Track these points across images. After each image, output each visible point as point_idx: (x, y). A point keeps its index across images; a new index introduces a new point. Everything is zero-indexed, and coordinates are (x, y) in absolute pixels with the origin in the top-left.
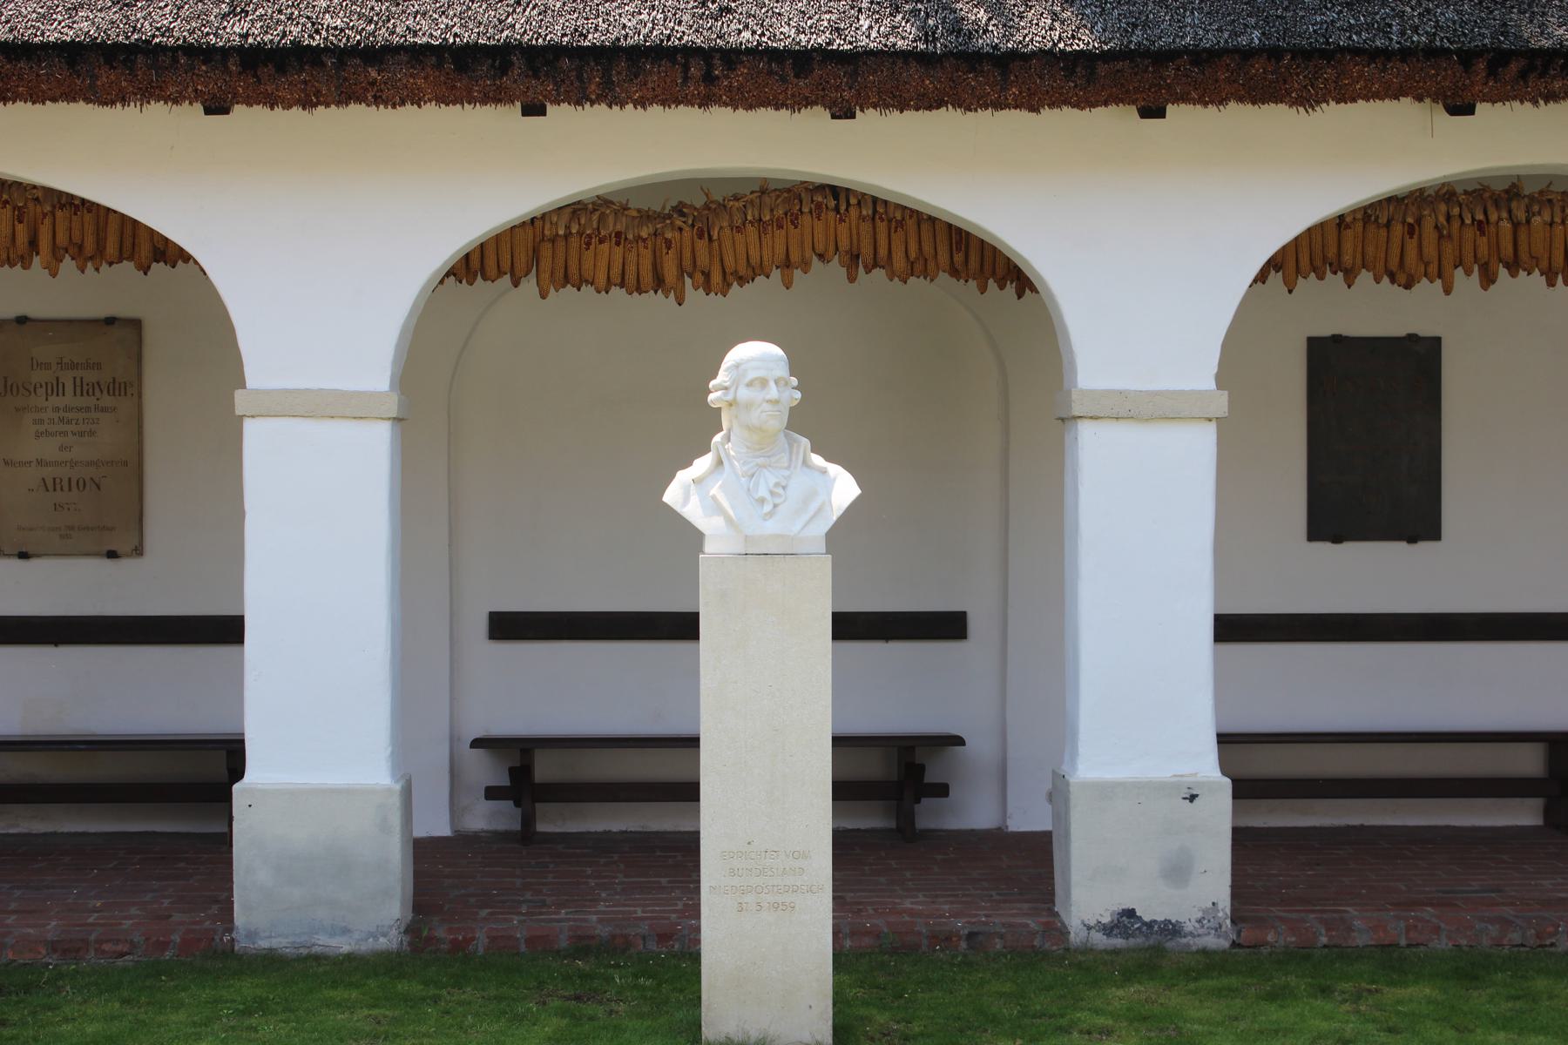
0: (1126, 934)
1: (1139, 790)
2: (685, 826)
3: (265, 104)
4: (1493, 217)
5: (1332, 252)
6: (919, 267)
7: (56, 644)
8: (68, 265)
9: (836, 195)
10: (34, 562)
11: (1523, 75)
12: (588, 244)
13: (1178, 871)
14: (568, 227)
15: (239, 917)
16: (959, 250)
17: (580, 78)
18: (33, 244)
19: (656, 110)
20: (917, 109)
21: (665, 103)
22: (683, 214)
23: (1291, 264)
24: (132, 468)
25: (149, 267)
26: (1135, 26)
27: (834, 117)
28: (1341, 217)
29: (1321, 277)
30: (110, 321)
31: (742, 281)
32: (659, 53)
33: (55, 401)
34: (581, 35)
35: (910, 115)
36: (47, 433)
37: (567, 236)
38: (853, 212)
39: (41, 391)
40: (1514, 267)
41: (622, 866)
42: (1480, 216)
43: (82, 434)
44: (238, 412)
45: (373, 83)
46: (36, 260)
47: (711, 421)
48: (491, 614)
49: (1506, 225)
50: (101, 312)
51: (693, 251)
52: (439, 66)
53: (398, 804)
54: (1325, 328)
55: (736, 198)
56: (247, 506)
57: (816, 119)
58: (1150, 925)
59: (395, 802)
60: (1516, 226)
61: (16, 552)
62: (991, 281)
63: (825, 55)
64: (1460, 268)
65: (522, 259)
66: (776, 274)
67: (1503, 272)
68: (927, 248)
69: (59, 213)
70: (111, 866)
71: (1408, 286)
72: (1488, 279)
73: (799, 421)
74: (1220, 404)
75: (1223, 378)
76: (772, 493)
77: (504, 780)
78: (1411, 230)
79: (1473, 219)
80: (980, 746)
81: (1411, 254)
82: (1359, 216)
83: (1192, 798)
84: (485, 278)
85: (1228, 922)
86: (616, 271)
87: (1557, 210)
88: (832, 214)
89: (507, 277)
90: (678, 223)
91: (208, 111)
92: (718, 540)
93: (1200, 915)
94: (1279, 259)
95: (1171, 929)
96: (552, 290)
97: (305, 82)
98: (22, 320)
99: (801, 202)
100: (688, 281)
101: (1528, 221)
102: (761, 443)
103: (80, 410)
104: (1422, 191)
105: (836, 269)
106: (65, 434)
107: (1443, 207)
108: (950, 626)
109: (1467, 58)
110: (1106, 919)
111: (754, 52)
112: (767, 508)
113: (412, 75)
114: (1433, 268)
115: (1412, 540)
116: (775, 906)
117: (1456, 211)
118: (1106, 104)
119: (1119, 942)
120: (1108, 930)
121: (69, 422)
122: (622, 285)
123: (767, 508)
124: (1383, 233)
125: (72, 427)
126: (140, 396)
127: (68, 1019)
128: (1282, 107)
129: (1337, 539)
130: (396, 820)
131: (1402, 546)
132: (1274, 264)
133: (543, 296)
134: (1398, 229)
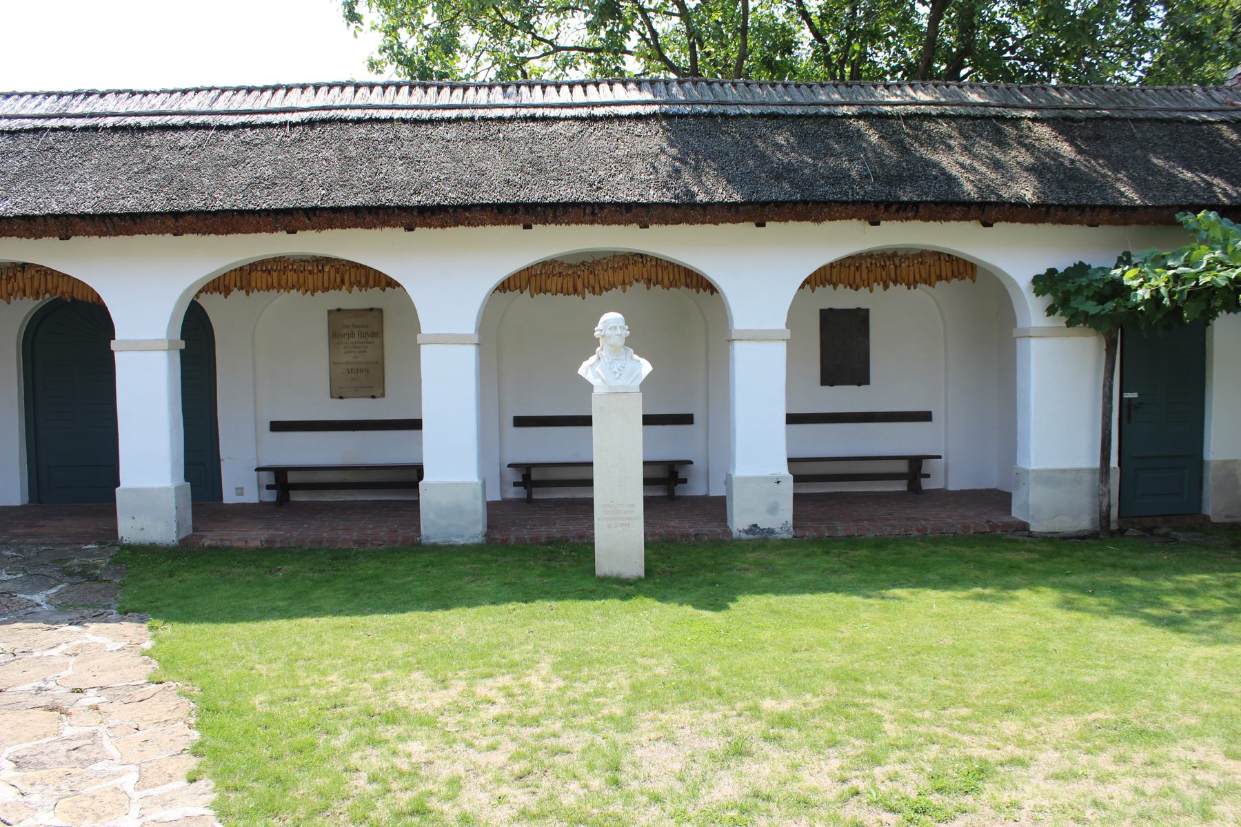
4: (888, 264)
6: (673, 284)
7: (354, 430)
8: (355, 289)
10: (345, 400)
11: (897, 211)
12: (269, 273)
13: (773, 510)
17: (545, 214)
18: (343, 282)
19: (573, 226)
23: (814, 282)
24: (380, 365)
29: (824, 286)
30: (371, 310)
31: (607, 290)
32: (575, 205)
35: (669, 226)
37: (541, 274)
40: (895, 282)
42: (883, 264)
44: (419, 342)
45: (467, 218)
46: (344, 287)
47: (596, 343)
48: (515, 417)
49: (892, 266)
50: (367, 306)
55: (604, 259)
57: (634, 228)
58: (763, 530)
59: (480, 488)
60: (896, 267)
63: (637, 205)
67: (891, 284)
68: (677, 277)
71: (857, 290)
73: (629, 342)
74: (788, 335)
77: (521, 480)
78: (857, 268)
80: (699, 464)
83: (778, 482)
84: (510, 290)
90: (583, 268)
95: (771, 531)
98: (339, 310)
100: (586, 290)
101: (900, 265)
103: (361, 343)
104: (861, 254)
105: (642, 285)
107: (869, 260)
108: (687, 419)
109: (877, 204)
110: (746, 528)
112: (618, 375)
114: (866, 283)
116: (622, 525)
117: (874, 262)
119: (751, 537)
120: (747, 532)
122: (562, 292)
123: (618, 375)
124: (847, 269)
126: (382, 337)
128: (809, 223)
129: (832, 385)
130: (480, 494)
131: (855, 387)
133: (532, 297)
134: (853, 268)
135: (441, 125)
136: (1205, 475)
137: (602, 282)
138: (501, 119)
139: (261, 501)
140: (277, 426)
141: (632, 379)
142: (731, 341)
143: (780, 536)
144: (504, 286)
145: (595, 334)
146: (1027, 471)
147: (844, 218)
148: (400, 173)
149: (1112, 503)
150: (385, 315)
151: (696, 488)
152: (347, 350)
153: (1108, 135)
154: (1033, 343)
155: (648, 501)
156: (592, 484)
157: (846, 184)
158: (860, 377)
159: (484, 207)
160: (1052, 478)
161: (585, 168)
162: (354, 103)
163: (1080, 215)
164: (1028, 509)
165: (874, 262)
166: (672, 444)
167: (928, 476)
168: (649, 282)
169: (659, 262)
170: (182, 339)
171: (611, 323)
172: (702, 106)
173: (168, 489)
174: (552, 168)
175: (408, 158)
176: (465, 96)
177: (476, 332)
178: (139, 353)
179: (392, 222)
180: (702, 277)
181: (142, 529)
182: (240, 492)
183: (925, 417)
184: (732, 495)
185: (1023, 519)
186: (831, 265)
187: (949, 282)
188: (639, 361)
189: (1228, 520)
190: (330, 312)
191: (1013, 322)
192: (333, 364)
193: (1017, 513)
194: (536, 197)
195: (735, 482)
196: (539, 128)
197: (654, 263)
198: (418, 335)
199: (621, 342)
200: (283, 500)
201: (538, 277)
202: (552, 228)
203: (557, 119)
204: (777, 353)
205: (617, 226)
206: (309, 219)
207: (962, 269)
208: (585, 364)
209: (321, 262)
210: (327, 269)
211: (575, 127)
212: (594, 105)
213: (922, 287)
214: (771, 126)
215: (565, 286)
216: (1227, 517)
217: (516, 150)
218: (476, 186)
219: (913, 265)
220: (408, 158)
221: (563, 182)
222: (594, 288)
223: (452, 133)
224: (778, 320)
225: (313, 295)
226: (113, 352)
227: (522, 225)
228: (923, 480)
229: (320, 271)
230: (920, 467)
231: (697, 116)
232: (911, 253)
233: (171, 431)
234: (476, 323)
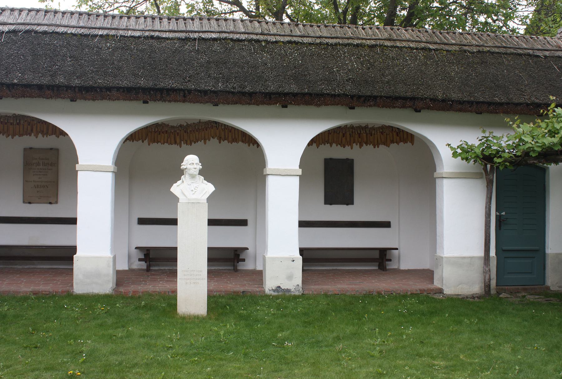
0: (278, 292)
1: (281, 260)
3: (84, 99)
4: (362, 132)
6: (234, 140)
8: (40, 135)
11: (364, 101)
12: (159, 134)
13: (290, 277)
14: (155, 129)
16: (244, 137)
18: (32, 130)
20: (232, 104)
22: (181, 127)
25: (59, 136)
26: (280, 87)
27: (213, 106)
29: (325, 145)
30: (51, 149)
32: (174, 90)
34: (156, 85)
40: (367, 144)
41: (166, 276)
42: (359, 132)
43: (44, 175)
44: (77, 169)
45: (108, 95)
46: (33, 134)
48: (138, 218)
49: (365, 135)
50: (50, 147)
51: (183, 135)
53: (112, 260)
54: (328, 157)
56: (78, 191)
58: (283, 290)
59: (111, 260)
61: (28, 202)
62: (251, 144)
64: (355, 144)
67: (364, 145)
69: (38, 124)
70: (69, 285)
73: (201, 173)
74: (300, 172)
76: (195, 189)
77: (143, 257)
78: (344, 135)
79: (358, 133)
80: (251, 251)
82: (333, 131)
83: (293, 261)
85: (301, 289)
87: (375, 131)
88: (215, 128)
89: (141, 141)
91: (71, 101)
92: (182, 199)
93: (295, 287)
95: (288, 290)
96: (151, 143)
97: (93, 95)
98: (31, 148)
99: (208, 124)
103: (44, 169)
104: (346, 126)
106: (40, 175)
107: (351, 130)
108: (243, 223)
109: (352, 97)
111: (196, 90)
112: (193, 192)
113: (117, 94)
115: (347, 204)
117: (354, 131)
119: (276, 294)
120: (274, 291)
121: (41, 172)
123: (193, 192)
126: (58, 166)
129: (331, 204)
130: (111, 264)
132: (311, 143)
133: (149, 145)
134: (341, 134)
136: (547, 262)
143: (293, 293)
145: (182, 167)
146: (442, 258)
149: (491, 278)
151: (248, 265)
152: (35, 173)
153: (488, 61)
154: (445, 181)
155: (209, 272)
156: (175, 260)
160: (458, 262)
161: (182, 69)
162: (44, 22)
163: (470, 107)
164: (443, 280)
165: (354, 131)
167: (390, 260)
168: (220, 139)
169: (226, 127)
172: (253, 35)
175: (74, 57)
176: (113, 22)
177: (112, 164)
183: (387, 225)
184: (265, 270)
190: (25, 149)
191: (434, 169)
193: (437, 284)
206: (10, 91)
207: (405, 136)
208: (175, 185)
210: (22, 122)
212: (189, 32)
213: (382, 147)
220: (74, 57)
221: (167, 77)
222: (186, 141)
224: (294, 164)
225: (13, 138)
227: (142, 101)
229: (18, 124)
230: (385, 255)
231: (250, 41)
234: (113, 159)
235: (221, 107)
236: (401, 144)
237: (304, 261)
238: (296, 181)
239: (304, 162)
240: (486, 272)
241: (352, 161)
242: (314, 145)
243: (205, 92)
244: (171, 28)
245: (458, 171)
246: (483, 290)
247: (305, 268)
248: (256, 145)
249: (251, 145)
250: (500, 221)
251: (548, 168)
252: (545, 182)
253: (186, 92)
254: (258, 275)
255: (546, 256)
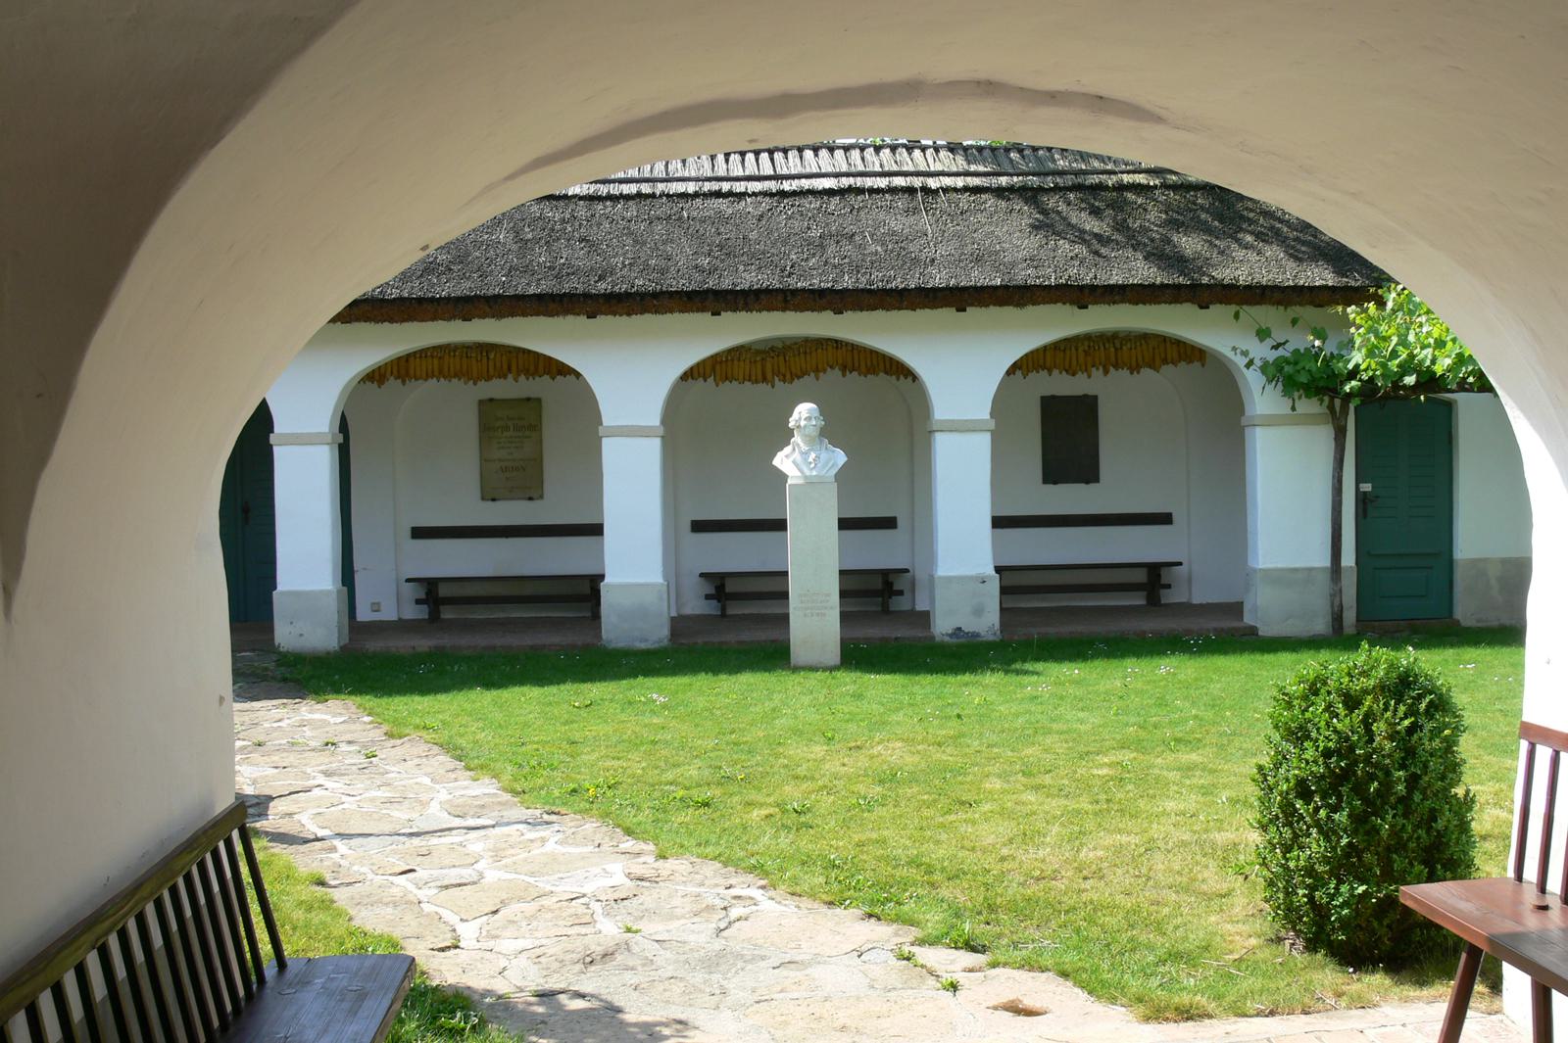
1: (962, 580)
2: (778, 611)
5: (1041, 362)
6: (871, 370)
7: (507, 537)
9: (837, 343)
10: (498, 503)
13: (978, 612)
15: (604, 635)
17: (736, 302)
18: (510, 370)
19: (765, 313)
21: (769, 310)
22: (773, 351)
23: (1025, 367)
24: (537, 462)
28: (1045, 347)
29: (1038, 372)
30: (528, 399)
31: (799, 378)
32: (768, 291)
33: (505, 434)
35: (865, 313)
36: (503, 448)
37: (727, 360)
38: (844, 348)
39: (500, 430)
40: (1116, 367)
45: (655, 306)
47: (790, 433)
49: (1112, 350)
50: (524, 395)
52: (680, 298)
55: (796, 344)
57: (828, 315)
58: (968, 633)
59: (665, 588)
60: (1116, 349)
63: (831, 291)
65: (708, 371)
66: (812, 374)
68: (875, 362)
71: (1073, 375)
72: (1106, 372)
74: (992, 425)
75: (663, 422)
77: (713, 592)
81: (1074, 362)
83: (984, 582)
84: (693, 378)
86: (747, 373)
90: (772, 355)
94: (1019, 363)
98: (491, 400)
100: (776, 379)
101: (1121, 348)
102: (810, 441)
103: (516, 437)
105: (837, 372)
106: (509, 448)
107: (1086, 343)
108: (889, 523)
110: (950, 632)
112: (813, 465)
114: (1084, 368)
115: (1087, 483)
116: (818, 614)
118: (942, 307)
119: (954, 640)
120: (951, 635)
121: (511, 442)
122: (749, 380)
123: (813, 465)
124: (1062, 353)
125: (514, 445)
127: (1114, 162)
128: (1011, 307)
129: (1055, 483)
131: (1083, 485)
132: (1012, 370)
133: (717, 386)
135: (620, 203)
137: (793, 370)
138: (684, 196)
139: (400, 619)
140: (419, 533)
141: (827, 468)
142: (931, 432)
143: (984, 639)
144: (689, 375)
146: (1255, 570)
147: (1048, 303)
148: (580, 257)
150: (544, 404)
154: (1258, 430)
157: (1050, 267)
158: (1089, 474)
159: (671, 294)
166: (877, 552)
167: (1169, 586)
168: (844, 369)
170: (340, 432)
171: (804, 413)
173: (329, 592)
174: (742, 252)
178: (305, 447)
179: (577, 310)
180: (902, 365)
181: (301, 635)
182: (376, 607)
183: (1165, 519)
185: (1253, 624)
186: (1045, 348)
187: (1176, 366)
188: (833, 451)
189: (1479, 625)
190: (481, 402)
191: (1242, 411)
192: (484, 461)
193: (1248, 619)
194: (726, 284)
195: (937, 581)
196: (721, 204)
197: (850, 348)
198: (271, 435)
199: (815, 433)
200: (434, 617)
201: (724, 365)
202: (743, 315)
203: (742, 195)
204: (981, 445)
205: (810, 312)
206: (490, 307)
209: (485, 349)
211: (764, 204)
213: (1146, 372)
214: (974, 202)
215: (753, 373)
216: (1478, 621)
217: (702, 231)
218: (663, 272)
219: (1135, 348)
222: (784, 376)
223: (632, 209)
226: (271, 446)
228: (1163, 592)
232: (1133, 334)
233: (333, 532)
235: (848, 315)
236: (1183, 364)
237: (1004, 591)
238: (654, 446)
239: (1001, 404)
240: (1337, 593)
241: (1095, 398)
242: (1019, 373)
243: (822, 293)
244: (747, 173)
245: (1285, 413)
246: (1331, 629)
247: (1004, 606)
248: (910, 379)
249: (902, 377)
250: (1363, 501)
251: (1456, 401)
252: (1450, 427)
253: (788, 294)
254: (925, 618)
255: (1455, 564)
